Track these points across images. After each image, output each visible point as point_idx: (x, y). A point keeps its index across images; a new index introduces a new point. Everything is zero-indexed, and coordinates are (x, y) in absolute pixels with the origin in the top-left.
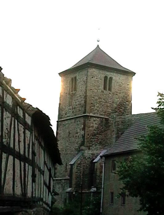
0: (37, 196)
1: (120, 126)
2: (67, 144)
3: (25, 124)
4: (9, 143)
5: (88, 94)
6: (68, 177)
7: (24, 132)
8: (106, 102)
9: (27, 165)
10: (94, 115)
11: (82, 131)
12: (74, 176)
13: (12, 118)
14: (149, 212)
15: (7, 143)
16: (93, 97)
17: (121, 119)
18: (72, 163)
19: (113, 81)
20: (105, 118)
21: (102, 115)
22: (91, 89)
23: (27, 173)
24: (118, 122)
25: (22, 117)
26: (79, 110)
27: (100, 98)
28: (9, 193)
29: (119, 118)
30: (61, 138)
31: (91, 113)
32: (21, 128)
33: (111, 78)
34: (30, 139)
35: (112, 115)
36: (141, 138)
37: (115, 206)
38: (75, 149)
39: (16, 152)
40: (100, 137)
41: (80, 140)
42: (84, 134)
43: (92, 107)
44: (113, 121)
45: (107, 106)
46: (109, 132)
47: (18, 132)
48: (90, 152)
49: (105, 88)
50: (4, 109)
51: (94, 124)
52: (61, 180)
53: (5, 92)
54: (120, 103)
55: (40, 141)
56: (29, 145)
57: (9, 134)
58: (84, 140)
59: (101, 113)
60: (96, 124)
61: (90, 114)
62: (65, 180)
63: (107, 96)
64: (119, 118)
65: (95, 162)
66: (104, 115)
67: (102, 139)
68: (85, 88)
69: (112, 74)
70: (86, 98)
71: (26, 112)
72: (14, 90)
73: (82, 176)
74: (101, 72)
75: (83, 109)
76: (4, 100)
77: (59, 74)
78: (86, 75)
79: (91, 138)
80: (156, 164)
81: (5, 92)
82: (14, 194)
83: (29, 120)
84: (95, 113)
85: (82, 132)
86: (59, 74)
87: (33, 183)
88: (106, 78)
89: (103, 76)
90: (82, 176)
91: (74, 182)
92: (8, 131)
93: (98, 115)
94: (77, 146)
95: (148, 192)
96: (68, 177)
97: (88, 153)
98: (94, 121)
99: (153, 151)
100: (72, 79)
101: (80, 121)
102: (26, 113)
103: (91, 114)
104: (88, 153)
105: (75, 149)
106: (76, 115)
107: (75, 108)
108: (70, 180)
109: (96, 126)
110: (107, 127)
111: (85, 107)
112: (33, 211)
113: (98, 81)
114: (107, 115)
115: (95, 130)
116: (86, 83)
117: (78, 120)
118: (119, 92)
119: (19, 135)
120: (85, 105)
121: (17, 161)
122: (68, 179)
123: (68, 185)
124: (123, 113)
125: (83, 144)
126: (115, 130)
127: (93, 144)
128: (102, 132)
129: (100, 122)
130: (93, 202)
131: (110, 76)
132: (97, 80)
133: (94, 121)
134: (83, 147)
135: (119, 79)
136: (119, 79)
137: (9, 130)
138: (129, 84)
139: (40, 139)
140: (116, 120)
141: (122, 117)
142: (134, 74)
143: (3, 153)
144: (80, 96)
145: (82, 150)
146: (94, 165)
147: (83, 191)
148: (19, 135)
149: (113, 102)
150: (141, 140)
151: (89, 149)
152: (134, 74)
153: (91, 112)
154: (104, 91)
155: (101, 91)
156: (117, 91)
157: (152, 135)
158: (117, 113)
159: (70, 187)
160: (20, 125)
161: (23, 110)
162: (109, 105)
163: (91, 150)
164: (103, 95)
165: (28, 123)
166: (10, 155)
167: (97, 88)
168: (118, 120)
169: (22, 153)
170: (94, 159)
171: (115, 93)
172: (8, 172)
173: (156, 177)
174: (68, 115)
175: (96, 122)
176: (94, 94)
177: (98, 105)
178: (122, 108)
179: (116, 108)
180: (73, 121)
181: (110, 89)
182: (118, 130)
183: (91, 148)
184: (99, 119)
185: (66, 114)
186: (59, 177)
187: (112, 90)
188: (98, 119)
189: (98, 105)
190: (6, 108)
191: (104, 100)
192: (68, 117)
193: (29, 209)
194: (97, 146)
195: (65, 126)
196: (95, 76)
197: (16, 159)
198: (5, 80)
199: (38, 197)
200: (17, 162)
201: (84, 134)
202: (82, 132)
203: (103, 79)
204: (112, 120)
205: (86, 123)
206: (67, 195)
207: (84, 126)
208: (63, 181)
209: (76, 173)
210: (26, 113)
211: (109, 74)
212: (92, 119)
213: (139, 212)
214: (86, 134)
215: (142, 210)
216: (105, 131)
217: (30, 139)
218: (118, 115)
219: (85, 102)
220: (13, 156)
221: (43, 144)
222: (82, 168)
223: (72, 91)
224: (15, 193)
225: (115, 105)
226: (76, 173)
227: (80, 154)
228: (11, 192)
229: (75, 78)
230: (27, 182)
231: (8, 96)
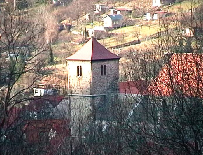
8: (103, 84)
10: (97, 95)
11: (90, 106)
19: (107, 68)
21: (101, 93)
26: (86, 91)
27: (99, 82)
31: (95, 94)
33: (105, 66)
35: (107, 92)
45: (104, 86)
59: (101, 92)
60: (98, 101)
61: (94, 95)
63: (103, 79)
66: (103, 93)
69: (105, 62)
80: (57, 93)
88: (102, 66)
93: (98, 95)
98: (97, 99)
101: (88, 99)
107: (82, 89)
113: (97, 71)
118: (110, 74)
128: (103, 105)
131: (104, 65)
132: (96, 70)
133: (97, 99)
135: (110, 65)
136: (110, 65)
138: (114, 77)
153: (95, 93)
155: (88, 3)
156: (109, 74)
162: (105, 85)
167: (97, 76)
174: (77, 92)
177: (98, 87)
181: (105, 74)
184: (100, 97)
185: (75, 91)
187: (107, 74)
188: (100, 97)
189: (98, 87)
196: (95, 68)
203: (100, 68)
211: (103, 64)
213: (77, 49)
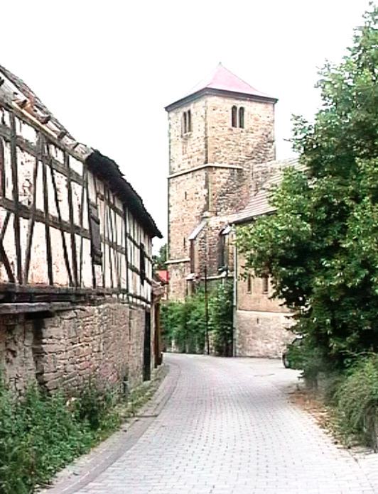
0: (108, 284)
1: (260, 179)
2: (184, 211)
3: (69, 174)
4: (32, 203)
5: (209, 135)
6: (188, 259)
7: (69, 186)
8: (237, 145)
9: (78, 238)
12: (196, 256)
13: (37, 164)
14: (286, 299)
15: (29, 203)
16: (218, 139)
17: (260, 169)
18: (192, 237)
19: (245, 113)
20: (238, 169)
21: (232, 164)
22: (213, 127)
23: (78, 250)
24: (257, 172)
25: (62, 162)
26: (198, 160)
28: (40, 282)
29: (258, 167)
30: (175, 202)
32: (61, 180)
33: (242, 109)
34: (83, 194)
35: (246, 163)
36: (271, 189)
37: (254, 295)
38: (196, 217)
39: (50, 217)
40: (231, 196)
41: (203, 203)
42: (208, 194)
43: (217, 154)
44: (249, 172)
46: (244, 189)
47: (55, 186)
48: (219, 219)
49: (234, 124)
50: (17, 148)
51: (221, 178)
52: (178, 263)
53: (17, 120)
54: (257, 145)
55: (112, 201)
56: (81, 207)
57: (32, 189)
58: (208, 203)
59: (232, 161)
62: (184, 262)
64: (258, 167)
65: (226, 234)
67: (234, 200)
68: (204, 126)
70: (207, 141)
71: (17, 145)
72: (40, 119)
73: (208, 256)
74: (227, 100)
75: (204, 157)
76: (15, 133)
77: (166, 108)
78: (204, 107)
79: (218, 200)
81: (17, 120)
82: (51, 283)
83: (77, 167)
84: (221, 162)
85: (205, 192)
86: (166, 108)
87: (97, 268)
88: (234, 108)
89: (231, 106)
90: (208, 256)
91: (196, 266)
92: (30, 183)
94: (198, 212)
95: (284, 269)
96: (188, 259)
97: (214, 222)
98: (221, 173)
99: (287, 207)
100: (185, 114)
102: (70, 157)
103: (217, 164)
104: (214, 222)
105: (196, 217)
106: (194, 167)
107: (191, 157)
108: (192, 261)
109: (224, 181)
110: (240, 182)
111: (207, 154)
112: (99, 309)
114: (240, 164)
115: (223, 187)
116: (205, 119)
117: (197, 173)
118: (255, 128)
119: (56, 190)
120: (207, 151)
121: (55, 233)
122: (188, 262)
123: (189, 269)
124: (264, 159)
125: (206, 208)
126: (254, 185)
127: (222, 208)
129: (230, 175)
130: (223, 291)
133: (221, 173)
134: (207, 214)
136: (255, 109)
137: (32, 182)
139: (111, 197)
140: (254, 170)
141: (263, 165)
142: (276, 100)
143: (21, 218)
144: (198, 138)
145: (207, 217)
146: (224, 238)
147: (207, 278)
148: (56, 190)
149: (248, 144)
150: (272, 191)
151: (216, 215)
152: (276, 100)
154: (233, 128)
157: (287, 182)
158: (254, 161)
159: (192, 272)
160: (57, 174)
161: (64, 151)
162: (241, 148)
163: (218, 217)
164: (232, 135)
165: (76, 171)
166: (38, 221)
167: (222, 125)
168: (256, 170)
169: (65, 217)
170: (223, 230)
171: (250, 131)
172: (35, 248)
173: (294, 245)
175: (224, 175)
176: (219, 134)
178: (261, 153)
179: (252, 153)
180: (190, 175)
181: (241, 126)
182: (257, 185)
183: (218, 213)
185: (179, 167)
186: (175, 259)
188: (228, 171)
189: (225, 150)
190: (22, 146)
191: (234, 141)
192: (182, 170)
193: (90, 306)
194: (227, 210)
195: (179, 183)
197: (51, 228)
198: (17, 101)
199: (112, 287)
200: (54, 233)
201: (208, 194)
202: (205, 192)
204: (248, 170)
205: (210, 178)
206: (189, 284)
207: (207, 182)
208: (182, 264)
209: (200, 251)
210: (70, 157)
211: (239, 104)
212: (219, 171)
214: (210, 194)
215: (277, 297)
216: (238, 187)
217: (83, 194)
218: (256, 163)
219: (206, 146)
220: (44, 223)
221: (119, 206)
222: (207, 244)
223: (185, 132)
224: (54, 281)
225: (250, 149)
226: (200, 251)
227: (204, 223)
228: (46, 280)
229: (189, 112)
230: (81, 264)
231: (25, 127)
